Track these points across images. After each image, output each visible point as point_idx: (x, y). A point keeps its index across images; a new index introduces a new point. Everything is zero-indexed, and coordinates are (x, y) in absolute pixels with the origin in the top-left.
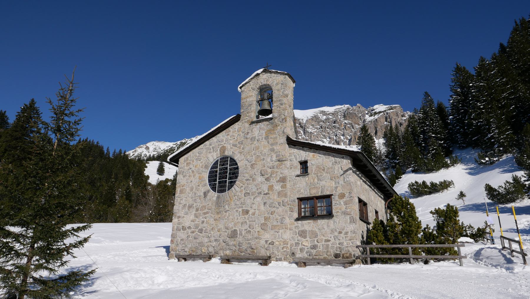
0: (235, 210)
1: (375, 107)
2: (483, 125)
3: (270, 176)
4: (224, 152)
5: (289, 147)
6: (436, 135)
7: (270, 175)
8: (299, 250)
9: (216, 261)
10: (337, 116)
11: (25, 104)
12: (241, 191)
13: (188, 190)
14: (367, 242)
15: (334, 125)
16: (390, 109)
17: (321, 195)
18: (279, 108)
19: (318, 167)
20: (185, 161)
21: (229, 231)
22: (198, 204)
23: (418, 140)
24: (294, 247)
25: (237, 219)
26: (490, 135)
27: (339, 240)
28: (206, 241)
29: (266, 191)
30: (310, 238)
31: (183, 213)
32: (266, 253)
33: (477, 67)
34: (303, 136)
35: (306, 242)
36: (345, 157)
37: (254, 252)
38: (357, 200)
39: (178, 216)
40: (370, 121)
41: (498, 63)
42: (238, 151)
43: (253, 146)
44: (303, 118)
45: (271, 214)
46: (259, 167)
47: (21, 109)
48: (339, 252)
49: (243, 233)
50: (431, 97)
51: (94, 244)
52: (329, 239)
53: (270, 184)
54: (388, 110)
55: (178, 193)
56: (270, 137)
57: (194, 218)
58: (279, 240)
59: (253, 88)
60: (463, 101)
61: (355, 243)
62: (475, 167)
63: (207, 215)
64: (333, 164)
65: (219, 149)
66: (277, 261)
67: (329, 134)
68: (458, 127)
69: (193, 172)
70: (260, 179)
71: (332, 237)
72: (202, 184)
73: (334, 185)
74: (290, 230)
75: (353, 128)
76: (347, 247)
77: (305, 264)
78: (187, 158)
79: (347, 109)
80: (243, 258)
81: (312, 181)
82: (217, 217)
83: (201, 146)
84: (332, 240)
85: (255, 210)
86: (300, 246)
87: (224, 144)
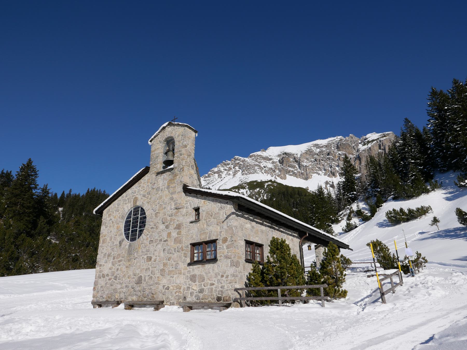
0: (141, 257)
1: (368, 136)
2: (460, 147)
4: (136, 203)
5: (186, 195)
6: (415, 161)
8: (189, 294)
9: (122, 306)
10: (331, 148)
11: (23, 164)
12: (147, 239)
13: (108, 239)
14: (250, 282)
15: (328, 157)
16: (383, 137)
17: (208, 240)
18: (179, 158)
19: (207, 213)
20: (107, 213)
21: (136, 278)
22: (115, 253)
23: (398, 167)
24: (186, 291)
25: (143, 265)
27: (221, 283)
28: (119, 288)
29: (166, 239)
30: (199, 283)
31: (103, 261)
33: (450, 90)
34: (299, 170)
35: (195, 286)
36: (228, 202)
37: (153, 297)
38: (243, 243)
40: (363, 150)
42: (146, 201)
43: (158, 195)
44: (297, 152)
45: (169, 260)
46: (161, 215)
47: (20, 169)
48: (220, 296)
49: (147, 278)
50: (411, 123)
51: (57, 291)
52: (214, 282)
54: (380, 138)
55: (101, 243)
56: (170, 187)
57: (111, 266)
58: (173, 285)
59: (160, 141)
60: (441, 124)
61: (233, 286)
62: (455, 191)
63: (121, 263)
65: (132, 200)
66: (171, 305)
67: (324, 166)
68: (437, 151)
70: (162, 227)
71: (216, 281)
72: (119, 234)
76: (227, 290)
77: (191, 308)
78: (109, 210)
79: (340, 140)
80: (140, 304)
82: (128, 264)
84: (216, 284)
86: (191, 290)
87: (137, 195)
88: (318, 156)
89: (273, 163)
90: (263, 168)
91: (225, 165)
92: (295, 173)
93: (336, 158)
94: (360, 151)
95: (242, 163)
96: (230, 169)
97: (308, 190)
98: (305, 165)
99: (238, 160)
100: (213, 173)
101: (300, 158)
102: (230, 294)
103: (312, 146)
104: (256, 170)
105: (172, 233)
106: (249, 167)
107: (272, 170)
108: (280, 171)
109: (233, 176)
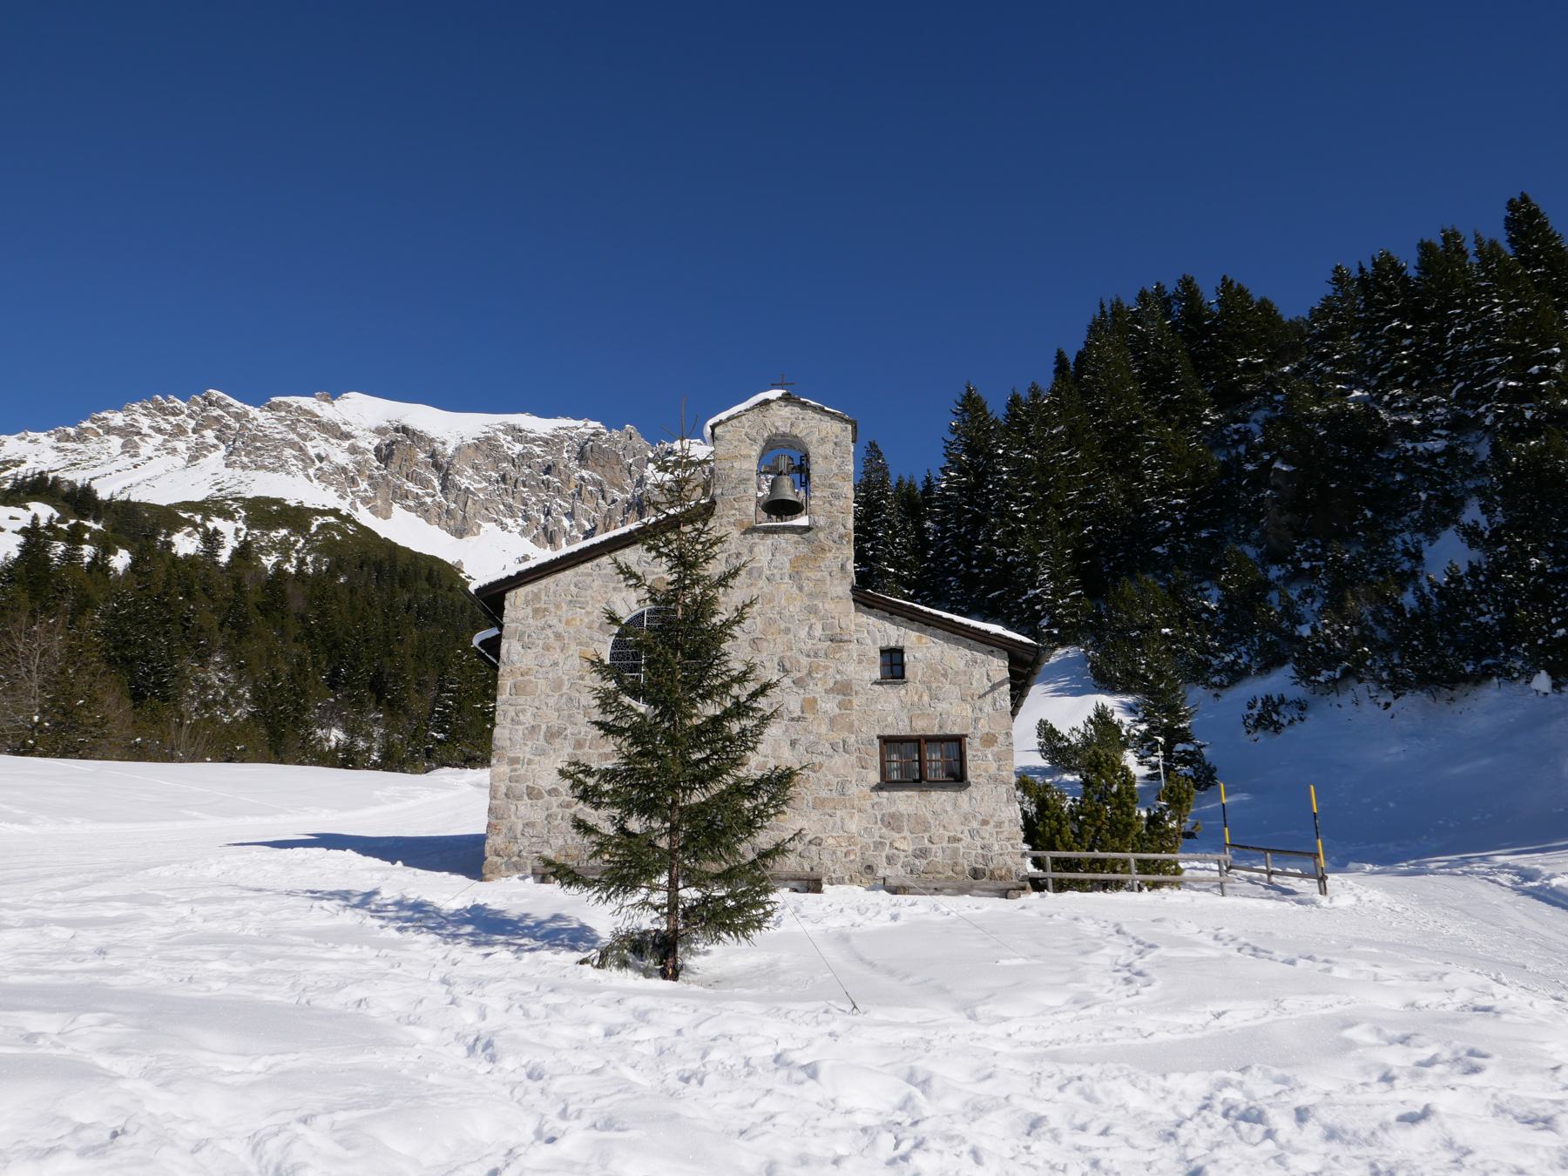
2: (1019, 564)
3: (807, 675)
5: (857, 610)
7: (805, 671)
8: (884, 860)
10: (560, 451)
15: (545, 477)
18: (827, 505)
20: (527, 603)
24: (871, 853)
26: (1033, 592)
29: (797, 713)
32: (801, 865)
34: (440, 498)
36: (996, 653)
39: (509, 758)
41: (1062, 405)
44: (447, 437)
48: (981, 866)
52: (961, 836)
53: (807, 696)
56: (804, 576)
64: (967, 664)
67: (526, 505)
68: (954, 558)
69: (558, 636)
71: (966, 832)
73: (970, 714)
74: (860, 811)
75: (603, 498)
76: (1001, 855)
78: (537, 596)
79: (593, 435)
81: (916, 698)
83: (587, 567)
85: (765, 756)
88: (514, 466)
89: (353, 450)
90: (313, 462)
91: (162, 410)
92: (424, 504)
93: (570, 489)
94: (648, 487)
95: (231, 421)
96: (180, 431)
97: (463, 572)
98: (463, 487)
99: (220, 407)
100: (101, 431)
101: (453, 457)
102: (1010, 863)
103: (502, 428)
104: (287, 462)
105: (819, 701)
106: (258, 444)
107: (346, 474)
108: (374, 484)
109: (189, 461)
